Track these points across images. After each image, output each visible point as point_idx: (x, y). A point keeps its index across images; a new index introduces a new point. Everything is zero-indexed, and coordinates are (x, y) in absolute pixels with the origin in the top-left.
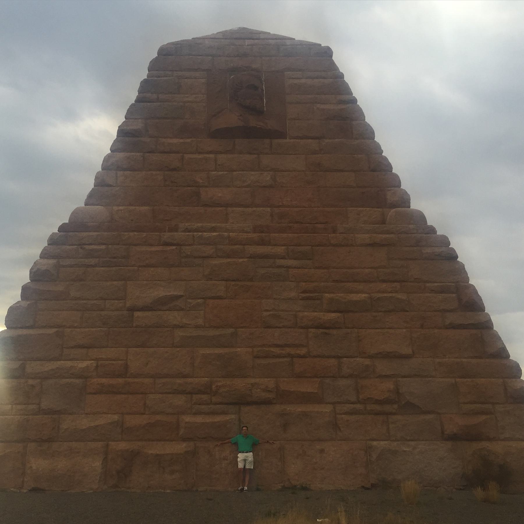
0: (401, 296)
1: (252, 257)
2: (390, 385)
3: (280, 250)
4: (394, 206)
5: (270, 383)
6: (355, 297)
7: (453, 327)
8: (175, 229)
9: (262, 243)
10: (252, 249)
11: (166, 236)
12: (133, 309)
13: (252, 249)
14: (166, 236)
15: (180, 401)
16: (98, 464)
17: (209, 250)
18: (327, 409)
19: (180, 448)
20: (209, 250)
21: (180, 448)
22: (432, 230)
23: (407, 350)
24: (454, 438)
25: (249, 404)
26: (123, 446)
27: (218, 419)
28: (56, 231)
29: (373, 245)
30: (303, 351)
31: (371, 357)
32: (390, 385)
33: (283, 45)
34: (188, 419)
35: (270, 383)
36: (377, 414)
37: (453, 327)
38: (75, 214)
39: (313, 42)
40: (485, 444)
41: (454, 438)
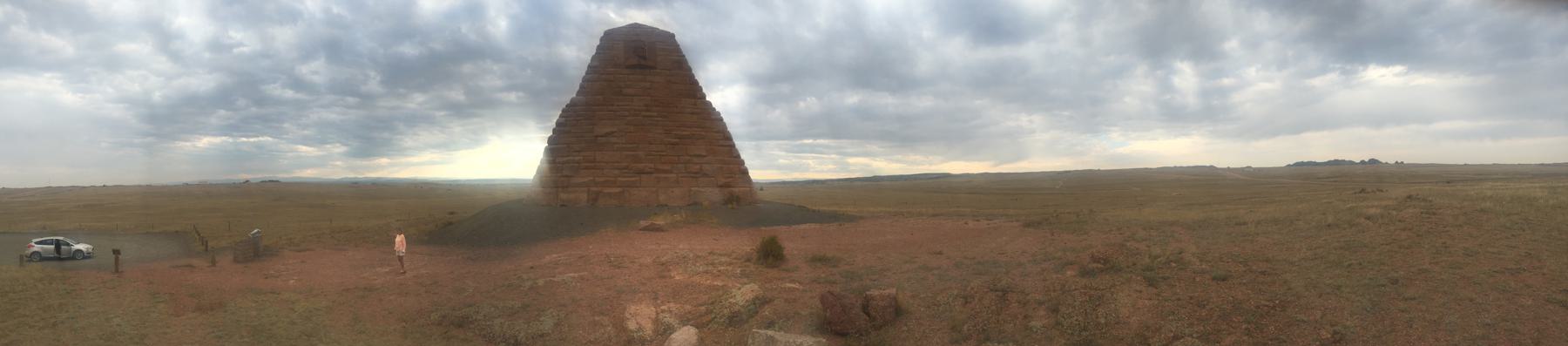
0: (703, 133)
1: (644, 116)
2: (698, 167)
3: (655, 114)
4: (700, 99)
5: (652, 165)
6: (684, 133)
7: (722, 146)
8: (613, 105)
9: (648, 111)
10: (644, 113)
11: (610, 108)
12: (597, 136)
13: (644, 113)
14: (610, 108)
15: (616, 172)
16: (585, 195)
17: (627, 113)
18: (674, 175)
19: (618, 190)
20: (627, 113)
21: (618, 190)
22: (714, 109)
23: (704, 154)
24: (721, 186)
25: (644, 173)
26: (595, 189)
27: (633, 179)
28: (574, 95)
29: (692, 113)
30: (664, 153)
31: (690, 156)
32: (698, 167)
33: (253, 252)
34: (620, 179)
35: (652, 165)
36: (693, 177)
37: (722, 146)
38: (572, 100)
39: (140, 186)
40: (733, 189)
41: (721, 186)
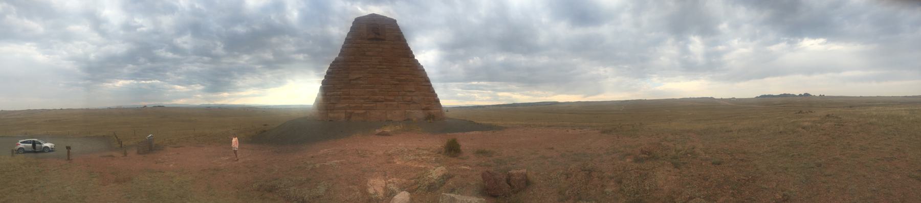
1: (378, 68)
2: (410, 98)
3: (385, 67)
4: (411, 58)
5: (383, 97)
6: (402, 78)
7: (424, 85)
8: (360, 62)
9: (380, 65)
10: (378, 66)
11: (358, 63)
12: (351, 80)
13: (378, 66)
14: (358, 63)
15: (362, 101)
16: (344, 115)
17: (368, 66)
18: (396, 103)
19: (363, 111)
20: (368, 66)
21: (363, 111)
22: (420, 64)
23: (414, 90)
24: (423, 109)
25: (378, 102)
26: (349, 111)
27: (372, 105)
28: (337, 56)
29: (407, 67)
30: (390, 90)
31: (406, 91)
32: (410, 98)
34: (364, 105)
35: (383, 97)
36: (407, 104)
37: (424, 85)
38: (336, 59)
39: (82, 109)
40: (431, 111)
41: (423, 109)
